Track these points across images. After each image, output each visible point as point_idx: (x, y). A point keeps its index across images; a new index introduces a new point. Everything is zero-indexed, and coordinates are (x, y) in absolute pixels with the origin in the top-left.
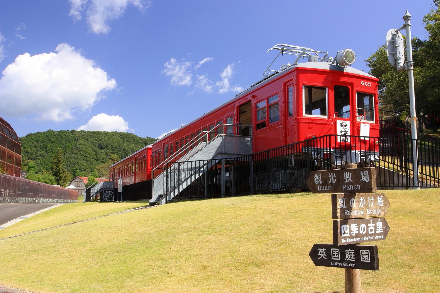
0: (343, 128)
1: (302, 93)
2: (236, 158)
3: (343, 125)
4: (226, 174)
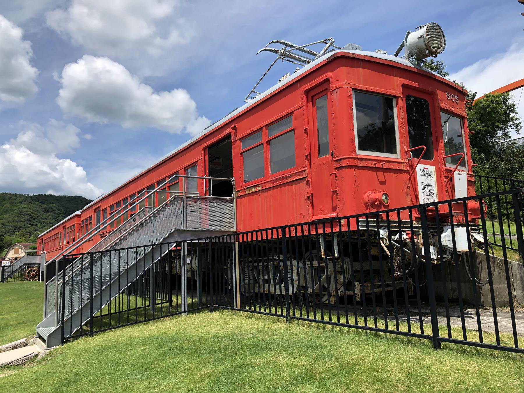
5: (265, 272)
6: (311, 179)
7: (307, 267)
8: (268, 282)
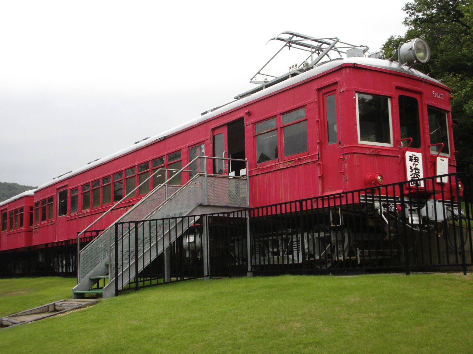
0: (414, 164)
1: (356, 106)
3: (413, 158)
4: (188, 238)
5: (261, 254)
6: (322, 162)
7: (315, 238)
8: (277, 254)
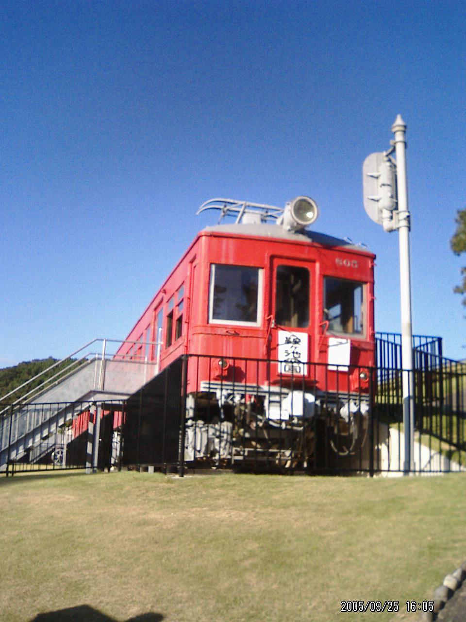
2: (122, 400)
